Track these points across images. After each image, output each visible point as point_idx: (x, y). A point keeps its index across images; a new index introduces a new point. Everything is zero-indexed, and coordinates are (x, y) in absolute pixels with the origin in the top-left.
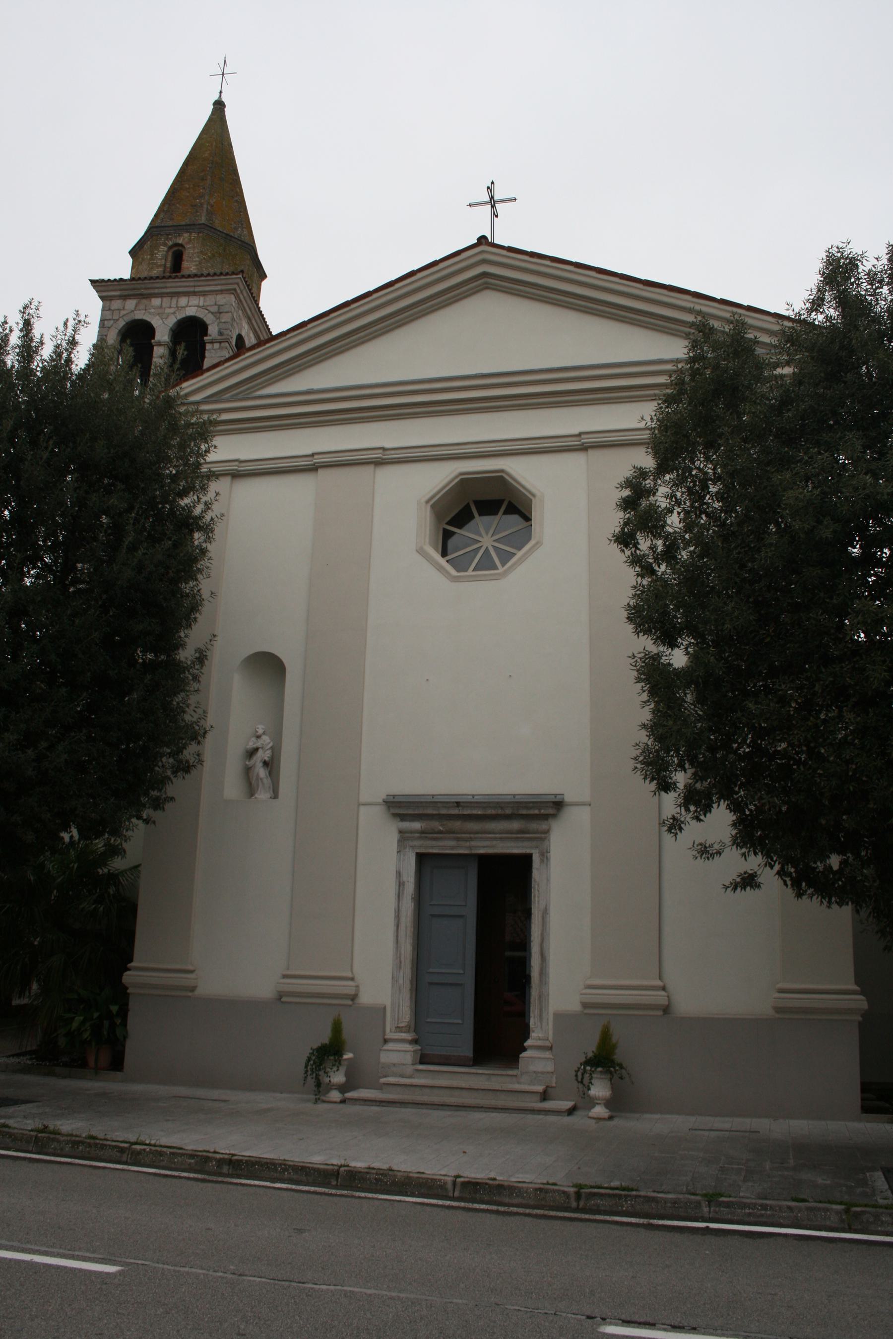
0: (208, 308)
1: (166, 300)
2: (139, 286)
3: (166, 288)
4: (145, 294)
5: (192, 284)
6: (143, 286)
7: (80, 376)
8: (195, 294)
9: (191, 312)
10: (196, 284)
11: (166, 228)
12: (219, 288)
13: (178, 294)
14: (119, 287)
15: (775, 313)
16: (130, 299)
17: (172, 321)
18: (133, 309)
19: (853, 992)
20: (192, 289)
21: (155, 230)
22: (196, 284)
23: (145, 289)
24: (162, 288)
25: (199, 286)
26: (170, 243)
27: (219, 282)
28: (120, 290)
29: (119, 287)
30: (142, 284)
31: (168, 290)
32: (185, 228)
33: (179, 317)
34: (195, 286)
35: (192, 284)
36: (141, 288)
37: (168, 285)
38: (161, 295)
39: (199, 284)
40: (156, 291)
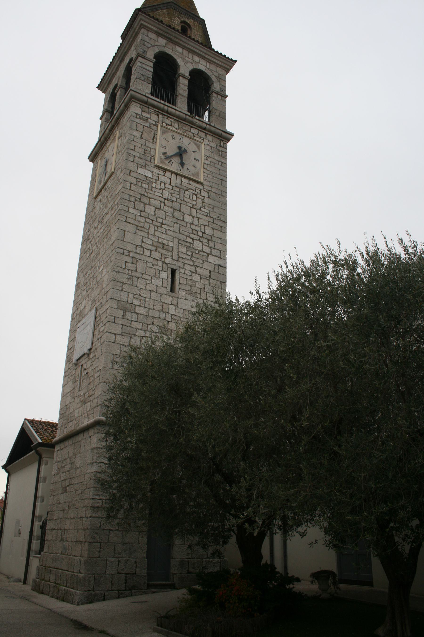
0: (213, 72)
1: (185, 52)
2: (171, 33)
3: (188, 44)
4: (173, 41)
5: (205, 51)
6: (174, 34)
7: (263, 564)
8: (204, 58)
9: (202, 68)
10: (208, 53)
11: (181, 9)
12: (220, 63)
13: (194, 53)
14: (157, 26)
15: (124, 36)
16: (162, 37)
17: (191, 67)
18: (164, 45)
19: (151, 72)
20: (203, 54)
21: (174, 5)
22: (208, 53)
23: (175, 37)
24: (185, 43)
25: (208, 55)
26: (182, 19)
27: (221, 60)
28: (158, 28)
29: (157, 26)
30: (174, 32)
31: (189, 47)
32: (192, 15)
33: (195, 67)
34: (206, 54)
35: (205, 51)
36: (172, 36)
37: (190, 43)
38: (183, 47)
39: (209, 54)
40: (181, 43)
